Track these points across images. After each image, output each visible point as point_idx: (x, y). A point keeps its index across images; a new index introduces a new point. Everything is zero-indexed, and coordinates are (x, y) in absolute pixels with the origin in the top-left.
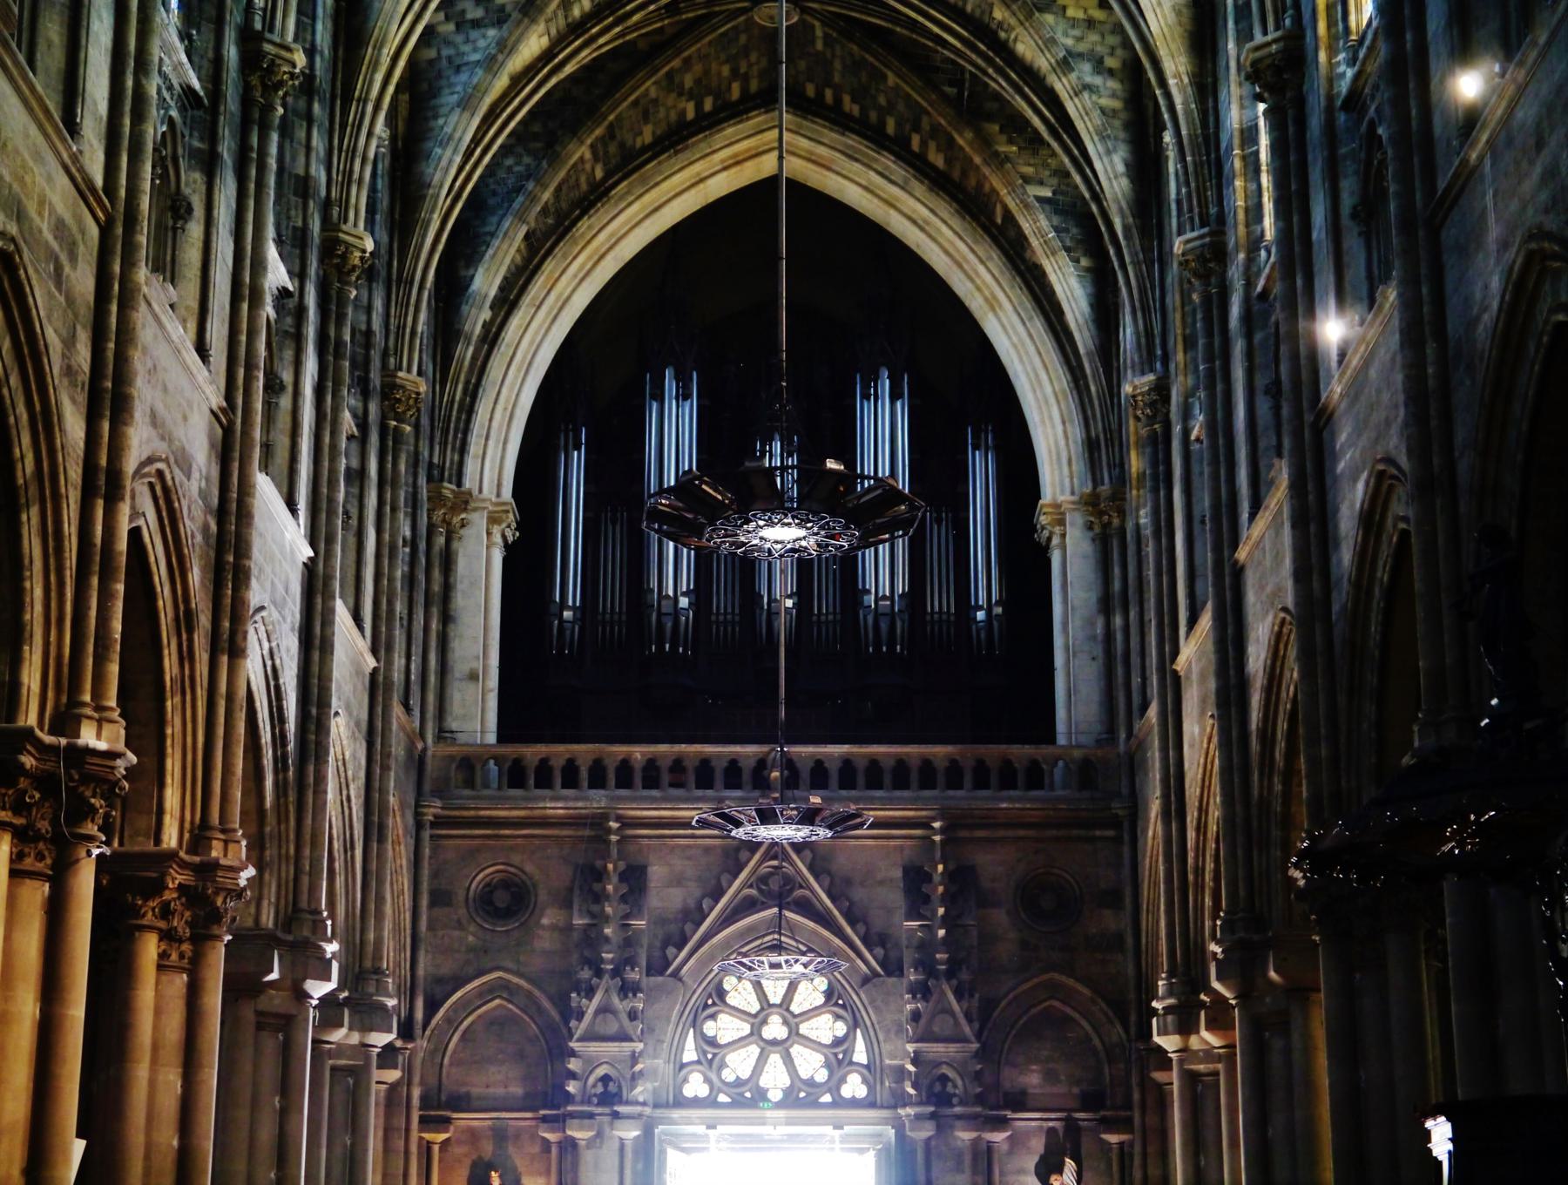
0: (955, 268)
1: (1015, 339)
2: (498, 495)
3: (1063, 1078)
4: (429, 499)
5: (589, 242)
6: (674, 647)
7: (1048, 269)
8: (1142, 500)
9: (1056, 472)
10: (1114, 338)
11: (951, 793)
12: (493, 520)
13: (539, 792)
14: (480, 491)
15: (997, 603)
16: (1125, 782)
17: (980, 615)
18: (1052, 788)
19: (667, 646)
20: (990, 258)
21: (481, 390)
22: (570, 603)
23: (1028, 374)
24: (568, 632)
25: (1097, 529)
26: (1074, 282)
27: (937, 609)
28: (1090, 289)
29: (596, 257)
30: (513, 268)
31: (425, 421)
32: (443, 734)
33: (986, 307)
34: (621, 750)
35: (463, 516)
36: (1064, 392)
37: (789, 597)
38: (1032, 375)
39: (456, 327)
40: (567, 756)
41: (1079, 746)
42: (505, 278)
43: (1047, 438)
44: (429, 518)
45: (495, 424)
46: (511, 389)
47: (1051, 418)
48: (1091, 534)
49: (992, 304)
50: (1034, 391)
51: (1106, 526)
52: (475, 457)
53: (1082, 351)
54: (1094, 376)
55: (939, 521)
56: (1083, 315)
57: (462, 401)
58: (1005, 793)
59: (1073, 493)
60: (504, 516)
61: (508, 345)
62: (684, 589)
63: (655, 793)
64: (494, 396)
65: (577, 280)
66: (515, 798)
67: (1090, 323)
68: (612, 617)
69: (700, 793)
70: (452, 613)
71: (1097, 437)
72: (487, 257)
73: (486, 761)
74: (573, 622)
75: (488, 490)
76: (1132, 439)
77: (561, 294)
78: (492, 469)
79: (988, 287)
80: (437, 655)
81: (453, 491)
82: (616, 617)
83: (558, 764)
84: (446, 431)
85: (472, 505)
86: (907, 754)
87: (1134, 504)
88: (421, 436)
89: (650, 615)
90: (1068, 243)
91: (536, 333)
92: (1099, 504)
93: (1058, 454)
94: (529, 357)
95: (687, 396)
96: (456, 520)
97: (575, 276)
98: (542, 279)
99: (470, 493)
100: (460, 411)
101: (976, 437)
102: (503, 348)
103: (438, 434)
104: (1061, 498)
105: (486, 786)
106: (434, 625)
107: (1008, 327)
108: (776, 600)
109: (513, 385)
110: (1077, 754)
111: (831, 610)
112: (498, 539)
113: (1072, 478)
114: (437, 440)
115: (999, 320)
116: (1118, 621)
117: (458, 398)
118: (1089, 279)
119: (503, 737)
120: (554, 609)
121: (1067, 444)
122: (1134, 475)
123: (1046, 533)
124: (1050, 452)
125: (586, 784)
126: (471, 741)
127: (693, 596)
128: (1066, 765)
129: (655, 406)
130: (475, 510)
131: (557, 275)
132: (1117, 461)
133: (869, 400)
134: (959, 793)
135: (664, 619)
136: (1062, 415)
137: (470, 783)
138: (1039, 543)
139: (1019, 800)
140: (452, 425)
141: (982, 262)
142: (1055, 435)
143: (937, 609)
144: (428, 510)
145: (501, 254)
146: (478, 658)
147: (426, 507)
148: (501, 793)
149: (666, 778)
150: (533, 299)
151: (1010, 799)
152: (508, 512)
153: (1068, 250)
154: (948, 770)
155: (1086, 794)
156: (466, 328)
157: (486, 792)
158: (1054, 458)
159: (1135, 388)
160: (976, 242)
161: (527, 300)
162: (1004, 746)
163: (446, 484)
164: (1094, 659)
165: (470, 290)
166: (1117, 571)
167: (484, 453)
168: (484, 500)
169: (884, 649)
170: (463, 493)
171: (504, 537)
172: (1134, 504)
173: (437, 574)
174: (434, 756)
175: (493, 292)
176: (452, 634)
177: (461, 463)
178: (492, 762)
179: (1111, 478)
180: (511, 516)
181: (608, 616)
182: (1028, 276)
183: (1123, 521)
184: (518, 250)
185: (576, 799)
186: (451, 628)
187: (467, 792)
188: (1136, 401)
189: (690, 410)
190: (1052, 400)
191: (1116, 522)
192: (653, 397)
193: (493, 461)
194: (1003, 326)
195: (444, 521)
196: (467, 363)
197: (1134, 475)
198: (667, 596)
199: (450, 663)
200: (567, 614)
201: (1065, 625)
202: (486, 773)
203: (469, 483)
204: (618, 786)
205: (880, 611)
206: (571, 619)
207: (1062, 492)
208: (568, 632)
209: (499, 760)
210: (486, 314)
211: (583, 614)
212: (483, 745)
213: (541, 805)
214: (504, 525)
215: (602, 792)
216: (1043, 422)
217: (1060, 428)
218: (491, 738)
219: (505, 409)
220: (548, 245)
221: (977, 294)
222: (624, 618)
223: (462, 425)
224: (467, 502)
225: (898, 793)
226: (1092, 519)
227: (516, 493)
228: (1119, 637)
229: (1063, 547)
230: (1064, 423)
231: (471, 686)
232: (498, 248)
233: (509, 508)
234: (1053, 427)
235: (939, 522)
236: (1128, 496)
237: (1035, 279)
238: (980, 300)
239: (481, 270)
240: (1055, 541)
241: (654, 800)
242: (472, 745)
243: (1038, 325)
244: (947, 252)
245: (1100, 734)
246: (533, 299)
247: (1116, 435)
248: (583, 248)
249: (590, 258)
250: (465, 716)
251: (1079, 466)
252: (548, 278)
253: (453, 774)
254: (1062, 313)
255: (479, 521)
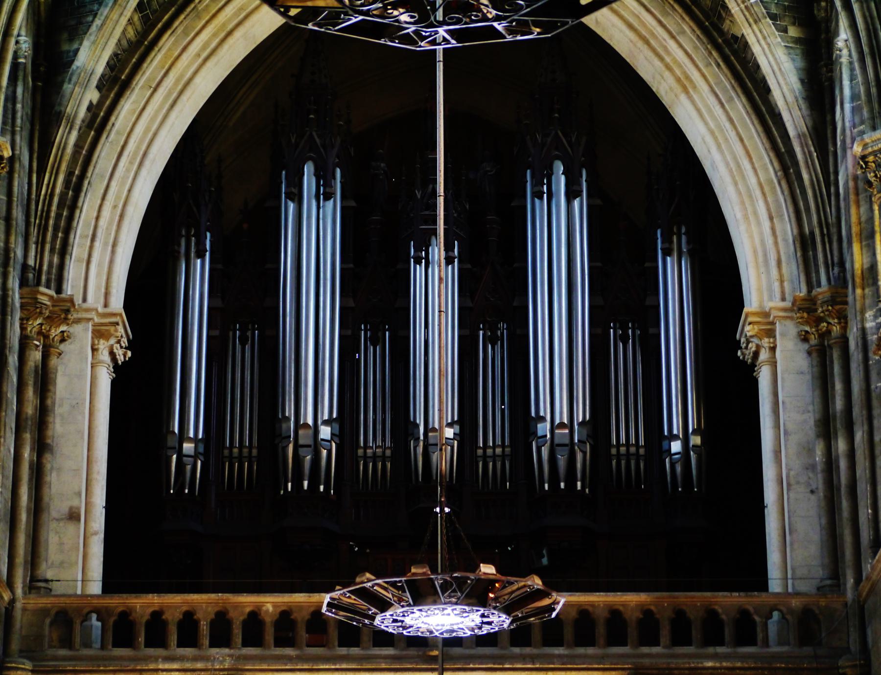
0: (640, 44)
1: (712, 125)
2: (106, 305)
3: (219, 327)
4: (23, 306)
5: (214, 16)
6: (314, 485)
7: (751, 39)
8: (868, 302)
9: (763, 277)
10: (829, 118)
11: (645, 650)
12: (99, 333)
13: (151, 651)
14: (85, 300)
15: (695, 432)
16: (854, 636)
17: (676, 447)
18: (766, 643)
19: (306, 483)
20: (683, 32)
21: (86, 182)
22: (191, 435)
23: (727, 164)
24: (189, 467)
25: (813, 340)
26: (781, 54)
27: (623, 440)
28: (800, 63)
29: (222, 35)
30: (124, 43)
31: (18, 214)
32: (35, 584)
33: (678, 89)
34: (248, 600)
35: (63, 328)
36: (770, 182)
37: (450, 425)
38: (732, 165)
39: (57, 108)
40: (184, 609)
41: (797, 594)
42: (115, 55)
43: (751, 237)
44: (23, 328)
45: (103, 222)
46: (123, 183)
47: (755, 213)
48: (806, 346)
49: (685, 85)
50: (736, 184)
51: (824, 335)
52: (79, 260)
53: (792, 133)
54: (806, 162)
55: (625, 339)
56: (792, 91)
57: (63, 195)
58: (711, 650)
59: (783, 299)
60: (112, 329)
61: (118, 133)
62: (326, 417)
63: (289, 651)
64: (102, 191)
65: (200, 60)
66: (121, 658)
67: (801, 101)
68: (250, 452)
69: (343, 651)
70: (49, 441)
71: (812, 233)
72: (94, 28)
73: (86, 618)
74: (195, 457)
75: (94, 299)
76: (855, 229)
77: (182, 76)
78: (98, 275)
79: (680, 66)
80: (30, 489)
81: (51, 298)
82: (245, 451)
83: (173, 617)
84: (43, 229)
85: (73, 316)
86: (592, 605)
87: (858, 306)
88: (13, 231)
89: (285, 449)
90: (774, 10)
91: (152, 120)
92: (816, 310)
93: (765, 255)
94: (144, 148)
95: (328, 196)
96: (54, 333)
97: (198, 55)
98: (159, 57)
99: (71, 301)
100: (60, 205)
101: (667, 240)
102: (112, 136)
103: (34, 232)
104: (769, 305)
105: (87, 644)
106: (27, 453)
107: (703, 110)
108: (434, 430)
109: (124, 178)
110: (795, 603)
111: (499, 442)
112: (105, 356)
113: (782, 282)
114: (33, 239)
115: (690, 98)
116: (841, 445)
117: (58, 190)
118: (798, 51)
119: (109, 586)
120: (172, 442)
121: (776, 243)
122: (858, 272)
123: (752, 347)
124: (755, 252)
125: (206, 642)
126: (70, 592)
127: (336, 426)
128: (783, 617)
129: (291, 206)
130: (78, 321)
131: (176, 54)
132: (836, 259)
133: (541, 198)
134: (655, 650)
135: (302, 451)
136: (769, 210)
137: (67, 642)
138: (744, 362)
139: (726, 657)
140: (51, 222)
141: (673, 37)
142: (761, 234)
143: (623, 440)
144: (21, 319)
145: (110, 24)
146: (79, 494)
147: (18, 315)
148: (104, 653)
149: (303, 634)
150: (149, 80)
151: (715, 657)
152: (117, 324)
153: (773, 17)
154: (640, 622)
155: (807, 650)
156: (68, 110)
157: (86, 652)
158: (761, 259)
159: (865, 146)
160: (665, 14)
161: (142, 80)
162: (709, 594)
163: (42, 289)
164: (812, 492)
165: (74, 67)
166: (839, 386)
167: (90, 255)
168: (88, 310)
169: (562, 485)
170: (64, 300)
171: (112, 354)
172: (858, 306)
173: (30, 393)
174: (24, 610)
175: (100, 69)
176: (48, 466)
177: (61, 267)
178: (94, 616)
179: (829, 280)
180: (120, 329)
181: (236, 451)
182: (727, 50)
183: (845, 328)
184: (130, 21)
185: (195, 659)
186: (49, 461)
187: (63, 652)
188: (866, 163)
189: (332, 209)
190: (758, 193)
191: (836, 329)
192: (290, 197)
193: (100, 265)
194: (698, 110)
195: (40, 333)
196: (69, 150)
197: (858, 272)
198: (306, 425)
199: (46, 499)
200: (188, 447)
201: (777, 453)
202: (87, 632)
203: (72, 287)
204: (245, 644)
205: (557, 441)
206: (192, 453)
207: (771, 299)
208: (189, 467)
209: (102, 614)
210: (93, 95)
211: (206, 448)
212: (84, 596)
213: (152, 666)
214: (112, 341)
215: (226, 651)
216: (746, 217)
217: (766, 224)
218: (96, 588)
219: (115, 207)
220: (166, 17)
221: (667, 74)
222: (255, 452)
223: (63, 223)
224: (67, 311)
225: (581, 650)
226: (807, 328)
227: (128, 305)
228: (843, 464)
229: (774, 364)
230: (771, 218)
231: (71, 527)
232: (107, 17)
233: (118, 319)
234: (759, 223)
235: (625, 339)
236: (850, 299)
237: (735, 53)
238: (671, 80)
239: (86, 43)
240: (764, 355)
241: (290, 659)
242: (70, 596)
243: (739, 107)
244: (631, 26)
245: (822, 580)
246: (149, 80)
247: (834, 230)
248: (208, 22)
249: (215, 35)
250: (62, 563)
251: (792, 269)
252: (166, 56)
253: (47, 632)
254: (768, 90)
255: (82, 334)
